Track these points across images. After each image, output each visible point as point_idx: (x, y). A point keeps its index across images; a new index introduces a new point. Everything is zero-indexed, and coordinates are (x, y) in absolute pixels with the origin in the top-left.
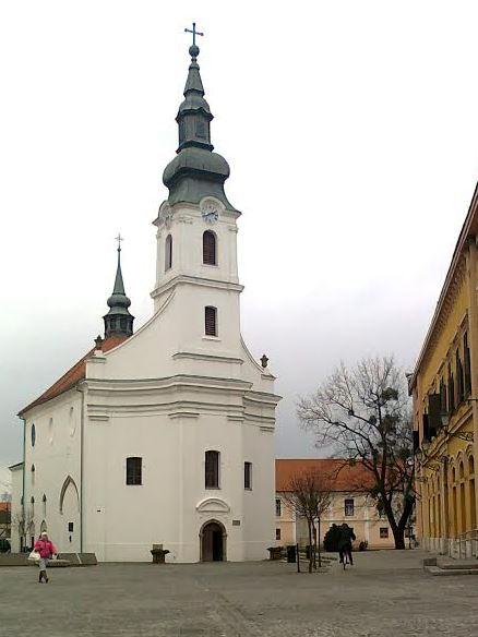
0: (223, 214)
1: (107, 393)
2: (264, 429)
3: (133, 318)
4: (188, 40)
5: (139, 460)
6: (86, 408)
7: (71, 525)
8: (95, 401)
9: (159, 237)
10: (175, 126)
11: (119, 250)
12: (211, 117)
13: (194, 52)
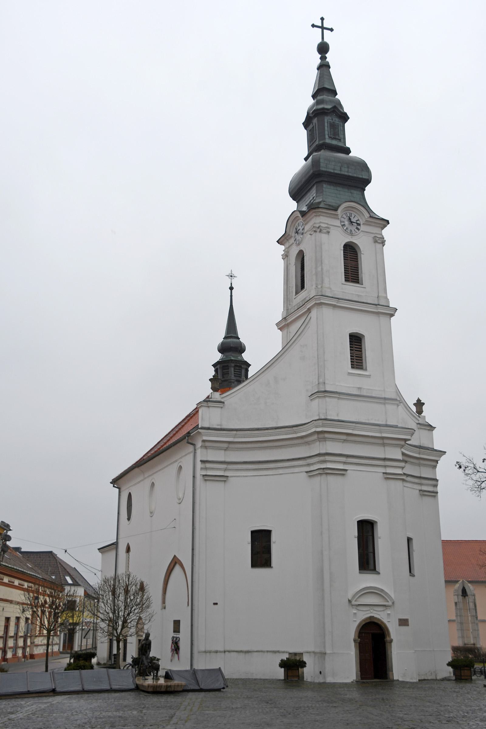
0: (367, 223)
1: (225, 445)
2: (423, 493)
3: (249, 365)
4: (316, 37)
5: (179, 621)
6: (199, 465)
7: (177, 624)
8: (212, 455)
9: (286, 256)
10: (304, 133)
11: (231, 288)
12: (345, 118)
13: (323, 49)
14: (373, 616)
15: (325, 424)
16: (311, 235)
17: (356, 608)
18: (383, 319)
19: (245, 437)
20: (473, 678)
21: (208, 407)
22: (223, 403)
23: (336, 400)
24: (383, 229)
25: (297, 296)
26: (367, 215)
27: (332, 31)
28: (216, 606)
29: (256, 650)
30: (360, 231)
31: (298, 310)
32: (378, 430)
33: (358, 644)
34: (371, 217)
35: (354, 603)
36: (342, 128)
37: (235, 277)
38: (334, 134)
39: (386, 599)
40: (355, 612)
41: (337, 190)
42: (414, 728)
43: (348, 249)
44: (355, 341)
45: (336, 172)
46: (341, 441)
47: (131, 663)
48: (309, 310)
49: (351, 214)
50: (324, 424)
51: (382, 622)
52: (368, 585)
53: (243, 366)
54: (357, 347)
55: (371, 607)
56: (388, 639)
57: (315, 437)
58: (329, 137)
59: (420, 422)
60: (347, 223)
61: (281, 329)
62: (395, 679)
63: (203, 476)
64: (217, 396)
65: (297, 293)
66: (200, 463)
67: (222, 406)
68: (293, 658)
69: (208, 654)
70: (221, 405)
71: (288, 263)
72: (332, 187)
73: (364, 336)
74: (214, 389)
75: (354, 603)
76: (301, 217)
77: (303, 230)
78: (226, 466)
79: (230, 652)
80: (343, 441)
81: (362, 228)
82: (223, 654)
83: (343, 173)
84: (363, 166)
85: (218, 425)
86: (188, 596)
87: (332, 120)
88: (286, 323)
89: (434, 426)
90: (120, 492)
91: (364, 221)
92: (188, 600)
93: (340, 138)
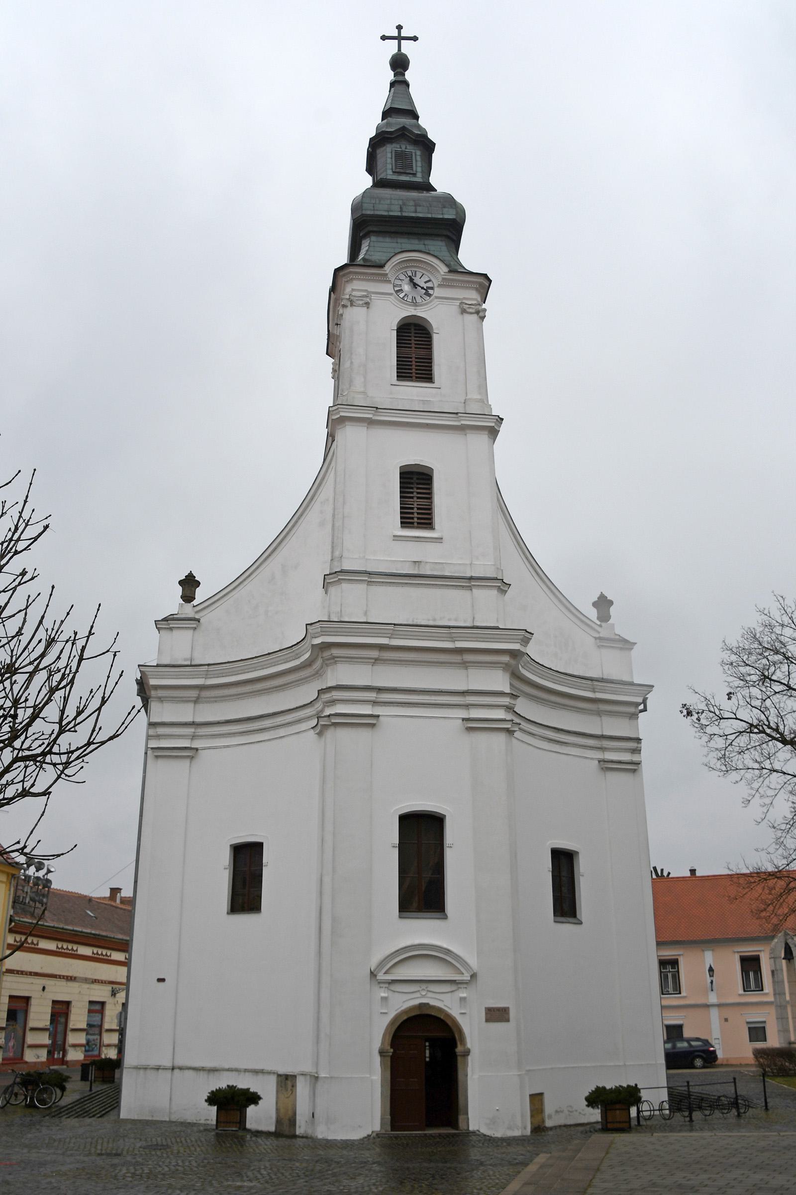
0: (445, 284)
1: (194, 693)
14: (428, 1004)
15: (328, 629)
17: (387, 988)
21: (171, 629)
22: (198, 620)
23: (363, 586)
28: (161, 984)
29: (227, 1067)
33: (389, 1059)
35: (381, 976)
40: (383, 995)
41: (397, 243)
42: (693, 1188)
44: (417, 481)
45: (391, 214)
46: (369, 662)
47: (64, 1084)
49: (416, 272)
51: (448, 1015)
55: (424, 986)
56: (459, 1049)
59: (601, 636)
60: (406, 288)
67: (195, 626)
69: (142, 1072)
72: (388, 240)
75: (381, 976)
78: (193, 730)
79: (183, 1069)
80: (373, 661)
81: (437, 292)
82: (168, 1074)
83: (405, 214)
85: (186, 660)
89: (632, 641)
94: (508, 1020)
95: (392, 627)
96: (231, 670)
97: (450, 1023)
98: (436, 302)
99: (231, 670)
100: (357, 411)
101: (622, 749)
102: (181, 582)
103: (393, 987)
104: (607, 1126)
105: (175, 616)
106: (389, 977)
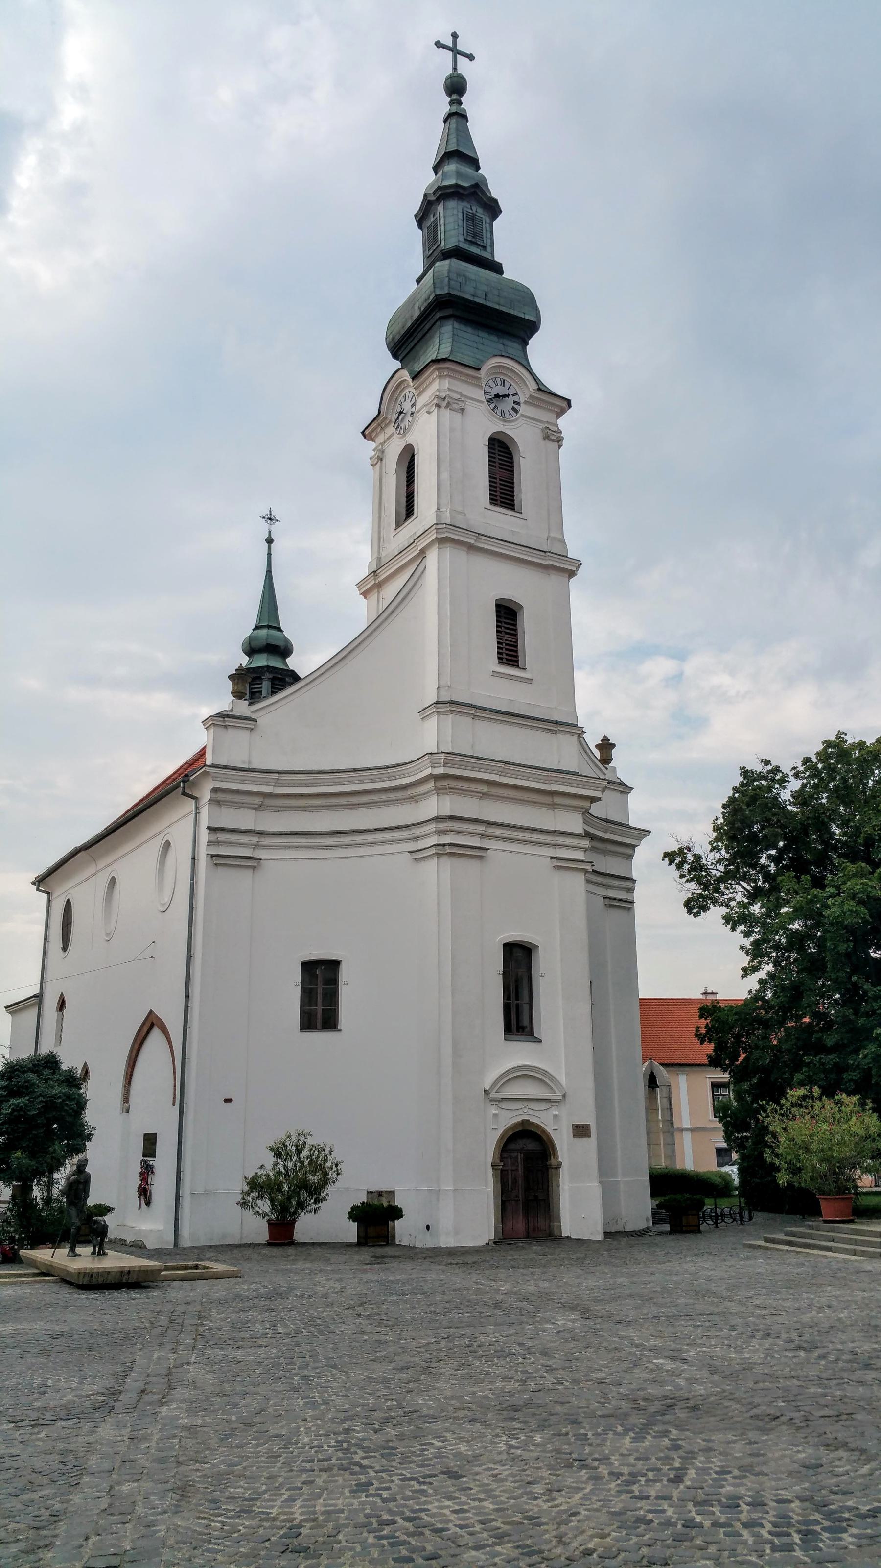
0: (532, 402)
1: (258, 800)
7: (150, 1142)
11: (270, 541)
12: (493, 209)
16: (429, 413)
18: (555, 579)
19: (296, 785)
20: (703, 1227)
21: (226, 727)
22: (256, 721)
23: (469, 720)
24: (559, 414)
25: (398, 530)
26: (533, 386)
27: (471, 60)
30: (519, 414)
31: (400, 555)
32: (546, 778)
34: (539, 389)
35: (493, 1095)
36: (488, 226)
37: (276, 520)
38: (475, 235)
39: (551, 1088)
43: (496, 447)
48: (423, 553)
50: (448, 761)
51: (544, 1131)
52: (521, 1063)
53: (287, 679)
54: (509, 626)
55: (526, 1104)
56: (553, 1162)
57: (431, 785)
58: (465, 239)
61: (365, 594)
62: (563, 1235)
63: (212, 856)
64: (243, 708)
65: (398, 524)
66: (207, 831)
67: (253, 727)
68: (376, 1202)
70: (250, 724)
71: (384, 471)
72: (469, 330)
73: (521, 607)
74: (238, 695)
75: (493, 1095)
76: (410, 380)
77: (412, 406)
78: (256, 839)
84: (527, 298)
85: (244, 762)
86: (175, 1086)
87: (472, 209)
88: (377, 581)
90: (49, 901)
91: (527, 396)
92: (175, 1094)
93: (484, 245)
94: (589, 1136)
95: (502, 765)
96: (305, 781)
97: (545, 1138)
98: (522, 421)
99: (305, 781)
100: (462, 534)
101: (620, 888)
102: (231, 677)
103: (504, 1105)
104: (363, 1241)
105: (229, 713)
106: (500, 1096)
